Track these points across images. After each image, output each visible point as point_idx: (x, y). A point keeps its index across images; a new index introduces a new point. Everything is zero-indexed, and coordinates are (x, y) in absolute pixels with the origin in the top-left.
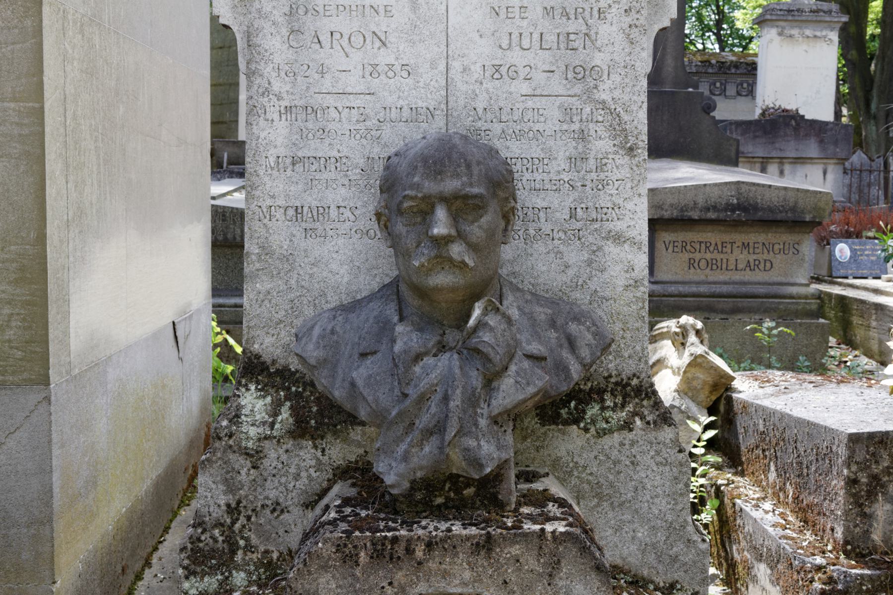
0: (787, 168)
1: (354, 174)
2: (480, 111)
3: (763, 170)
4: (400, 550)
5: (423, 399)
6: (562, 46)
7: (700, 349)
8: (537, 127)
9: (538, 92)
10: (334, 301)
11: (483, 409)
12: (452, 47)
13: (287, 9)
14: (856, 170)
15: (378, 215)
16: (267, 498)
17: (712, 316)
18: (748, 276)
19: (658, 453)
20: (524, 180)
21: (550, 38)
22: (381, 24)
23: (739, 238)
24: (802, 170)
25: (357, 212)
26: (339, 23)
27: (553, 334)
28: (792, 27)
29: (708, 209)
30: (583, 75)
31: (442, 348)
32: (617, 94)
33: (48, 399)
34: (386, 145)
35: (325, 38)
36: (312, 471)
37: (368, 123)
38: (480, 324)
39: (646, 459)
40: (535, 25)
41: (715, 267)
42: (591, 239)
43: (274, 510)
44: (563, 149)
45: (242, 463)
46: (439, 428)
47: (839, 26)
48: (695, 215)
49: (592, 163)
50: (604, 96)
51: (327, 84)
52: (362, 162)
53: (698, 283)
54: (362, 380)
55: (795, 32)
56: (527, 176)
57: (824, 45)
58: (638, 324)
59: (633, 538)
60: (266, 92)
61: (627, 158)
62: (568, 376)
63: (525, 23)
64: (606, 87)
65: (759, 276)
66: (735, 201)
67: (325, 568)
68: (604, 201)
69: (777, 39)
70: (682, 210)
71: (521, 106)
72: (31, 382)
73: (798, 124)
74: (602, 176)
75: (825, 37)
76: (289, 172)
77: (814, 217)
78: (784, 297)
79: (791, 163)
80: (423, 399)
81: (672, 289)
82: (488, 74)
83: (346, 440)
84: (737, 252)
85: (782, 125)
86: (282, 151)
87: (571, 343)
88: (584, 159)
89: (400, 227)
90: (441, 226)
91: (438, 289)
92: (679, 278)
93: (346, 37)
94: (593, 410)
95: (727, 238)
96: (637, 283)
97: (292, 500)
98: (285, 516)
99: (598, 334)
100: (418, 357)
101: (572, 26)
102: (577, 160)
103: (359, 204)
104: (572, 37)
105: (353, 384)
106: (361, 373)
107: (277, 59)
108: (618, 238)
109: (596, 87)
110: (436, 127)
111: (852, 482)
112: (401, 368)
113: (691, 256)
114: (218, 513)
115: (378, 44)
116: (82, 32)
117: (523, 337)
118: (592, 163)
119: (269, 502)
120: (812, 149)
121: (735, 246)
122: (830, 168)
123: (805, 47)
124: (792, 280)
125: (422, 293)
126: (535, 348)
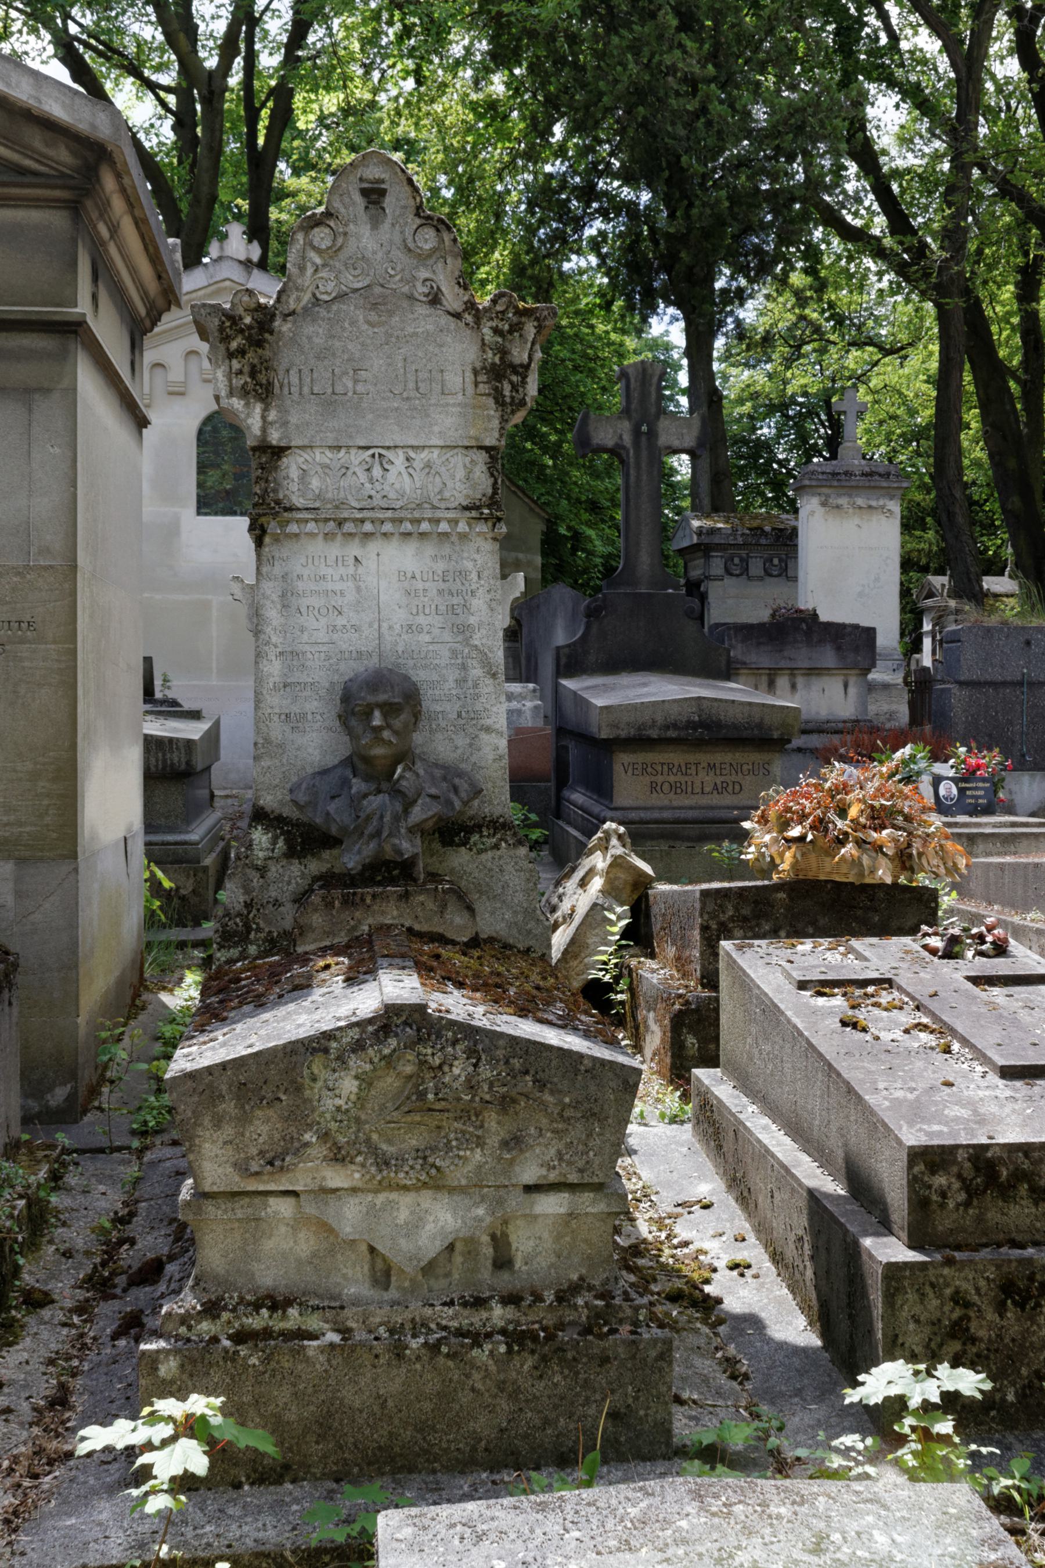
0: (800, 681)
1: (323, 692)
3: (771, 686)
4: (358, 899)
5: (368, 818)
7: (619, 851)
10: (310, 770)
11: (403, 824)
17: (678, 844)
18: (716, 800)
22: (339, 601)
23: (704, 758)
24: (818, 684)
27: (445, 785)
28: (839, 495)
29: (667, 727)
30: (463, 630)
31: (379, 791)
33: (76, 870)
35: (303, 610)
38: (401, 777)
39: (509, 868)
44: (452, 676)
45: (254, 875)
46: (378, 833)
48: (654, 734)
51: (305, 637)
53: (661, 808)
54: (336, 813)
55: (843, 501)
57: (883, 517)
60: (268, 643)
62: (453, 808)
67: (316, 910)
68: (478, 707)
69: (820, 511)
72: (64, 857)
73: (809, 628)
75: (883, 507)
80: (368, 818)
83: (320, 859)
84: (702, 774)
86: (277, 679)
87: (456, 789)
88: (465, 681)
89: (353, 722)
90: (377, 720)
91: (375, 757)
92: (640, 803)
94: (475, 838)
95: (691, 758)
96: (501, 757)
97: (286, 898)
99: (472, 784)
100: (365, 796)
101: (455, 601)
102: (461, 682)
105: (328, 814)
106: (332, 808)
107: (275, 623)
108: (488, 730)
110: (373, 663)
111: (705, 928)
112: (355, 802)
114: (239, 907)
117: (426, 785)
120: (828, 657)
122: (852, 680)
123: (857, 521)
125: (367, 760)
126: (433, 791)
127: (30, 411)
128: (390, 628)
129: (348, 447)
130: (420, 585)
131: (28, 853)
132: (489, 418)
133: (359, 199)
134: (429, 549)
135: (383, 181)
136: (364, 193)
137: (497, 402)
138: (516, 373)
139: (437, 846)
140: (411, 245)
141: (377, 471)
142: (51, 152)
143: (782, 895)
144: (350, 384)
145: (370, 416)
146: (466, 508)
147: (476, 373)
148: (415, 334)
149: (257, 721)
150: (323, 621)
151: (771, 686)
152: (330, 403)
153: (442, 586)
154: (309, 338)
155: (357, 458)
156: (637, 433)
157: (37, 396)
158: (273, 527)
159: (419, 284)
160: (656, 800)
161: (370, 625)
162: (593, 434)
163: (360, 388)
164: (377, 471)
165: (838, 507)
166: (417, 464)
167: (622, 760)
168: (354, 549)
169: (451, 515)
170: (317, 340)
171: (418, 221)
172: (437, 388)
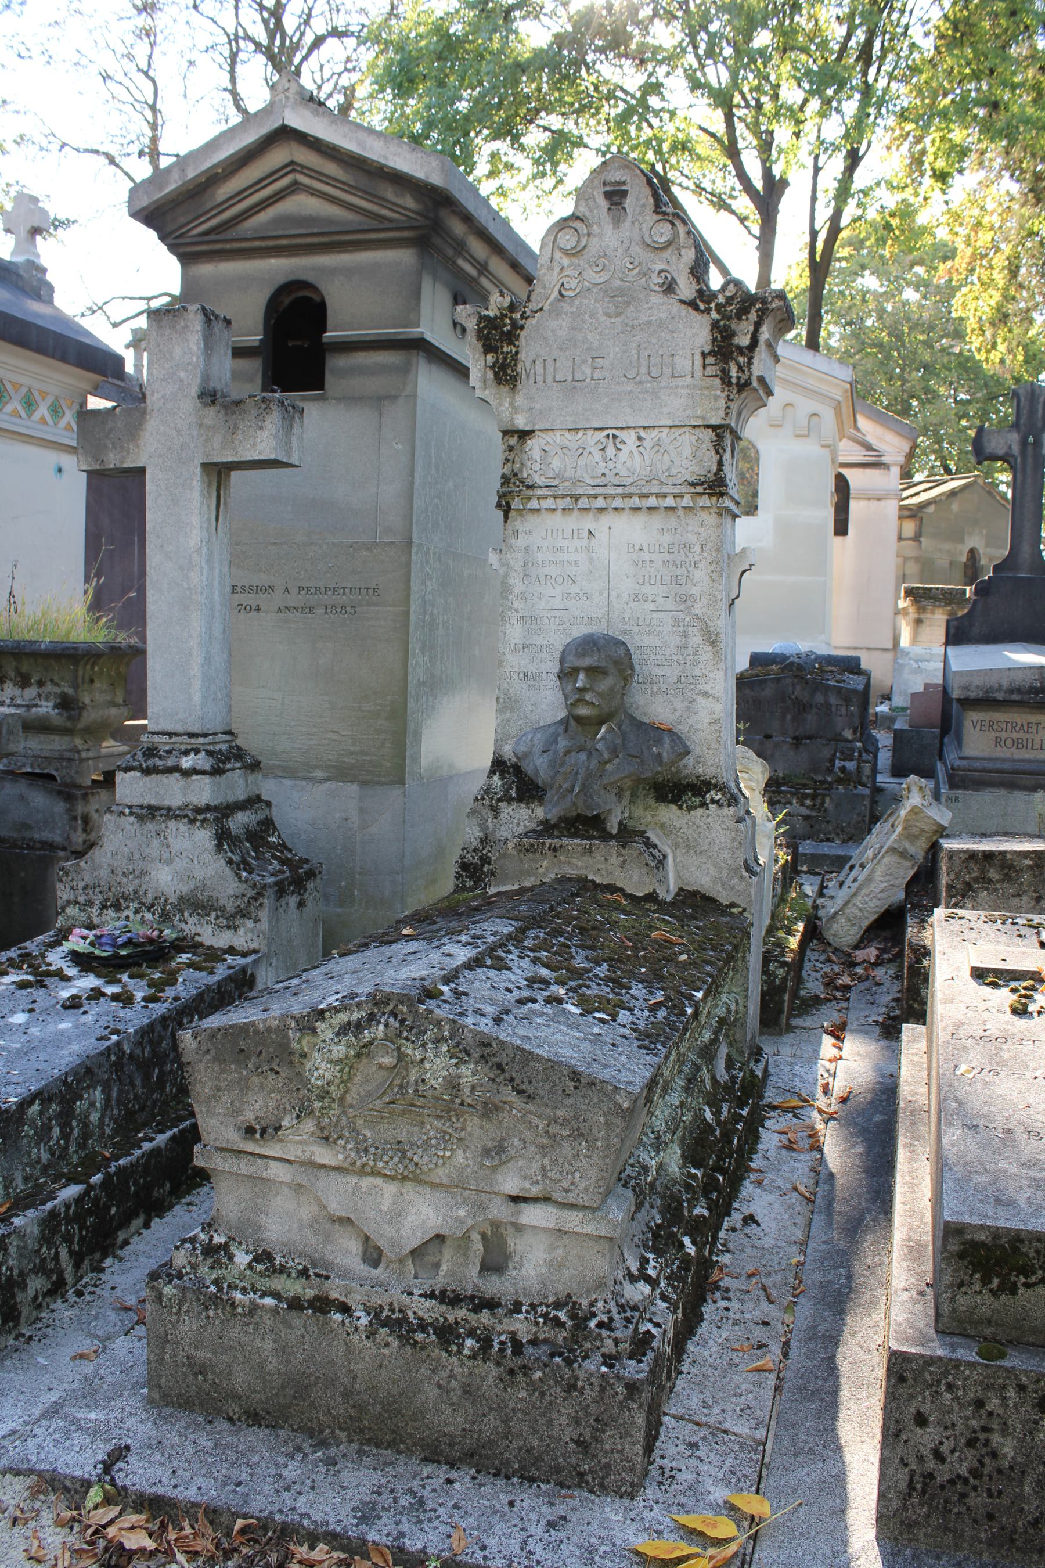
21: (667, 578)
26: (547, 571)
29: (1011, 691)
30: (685, 599)
32: (705, 610)
35: (542, 579)
44: (675, 641)
48: (1000, 696)
50: (698, 612)
51: (542, 604)
54: (539, 766)
56: (653, 657)
60: (510, 608)
68: (697, 673)
70: (987, 692)
81: (978, 765)
86: (518, 641)
99: (685, 746)
108: (706, 694)
116: (440, 560)
127: (381, 415)
128: (619, 596)
130: (647, 557)
131: (369, 778)
133: (604, 203)
134: (657, 521)
135: (624, 183)
136: (608, 195)
137: (723, 382)
138: (742, 353)
139: (651, 802)
140: (648, 241)
141: (610, 451)
142: (400, 201)
144: (588, 372)
145: (605, 400)
146: (693, 485)
147: (704, 355)
152: (572, 387)
154: (553, 331)
156: (1024, 443)
157: (386, 403)
159: (654, 276)
162: (986, 444)
164: (610, 451)
166: (647, 444)
168: (588, 522)
169: (676, 490)
170: (559, 333)
171: (656, 217)
172: (667, 371)
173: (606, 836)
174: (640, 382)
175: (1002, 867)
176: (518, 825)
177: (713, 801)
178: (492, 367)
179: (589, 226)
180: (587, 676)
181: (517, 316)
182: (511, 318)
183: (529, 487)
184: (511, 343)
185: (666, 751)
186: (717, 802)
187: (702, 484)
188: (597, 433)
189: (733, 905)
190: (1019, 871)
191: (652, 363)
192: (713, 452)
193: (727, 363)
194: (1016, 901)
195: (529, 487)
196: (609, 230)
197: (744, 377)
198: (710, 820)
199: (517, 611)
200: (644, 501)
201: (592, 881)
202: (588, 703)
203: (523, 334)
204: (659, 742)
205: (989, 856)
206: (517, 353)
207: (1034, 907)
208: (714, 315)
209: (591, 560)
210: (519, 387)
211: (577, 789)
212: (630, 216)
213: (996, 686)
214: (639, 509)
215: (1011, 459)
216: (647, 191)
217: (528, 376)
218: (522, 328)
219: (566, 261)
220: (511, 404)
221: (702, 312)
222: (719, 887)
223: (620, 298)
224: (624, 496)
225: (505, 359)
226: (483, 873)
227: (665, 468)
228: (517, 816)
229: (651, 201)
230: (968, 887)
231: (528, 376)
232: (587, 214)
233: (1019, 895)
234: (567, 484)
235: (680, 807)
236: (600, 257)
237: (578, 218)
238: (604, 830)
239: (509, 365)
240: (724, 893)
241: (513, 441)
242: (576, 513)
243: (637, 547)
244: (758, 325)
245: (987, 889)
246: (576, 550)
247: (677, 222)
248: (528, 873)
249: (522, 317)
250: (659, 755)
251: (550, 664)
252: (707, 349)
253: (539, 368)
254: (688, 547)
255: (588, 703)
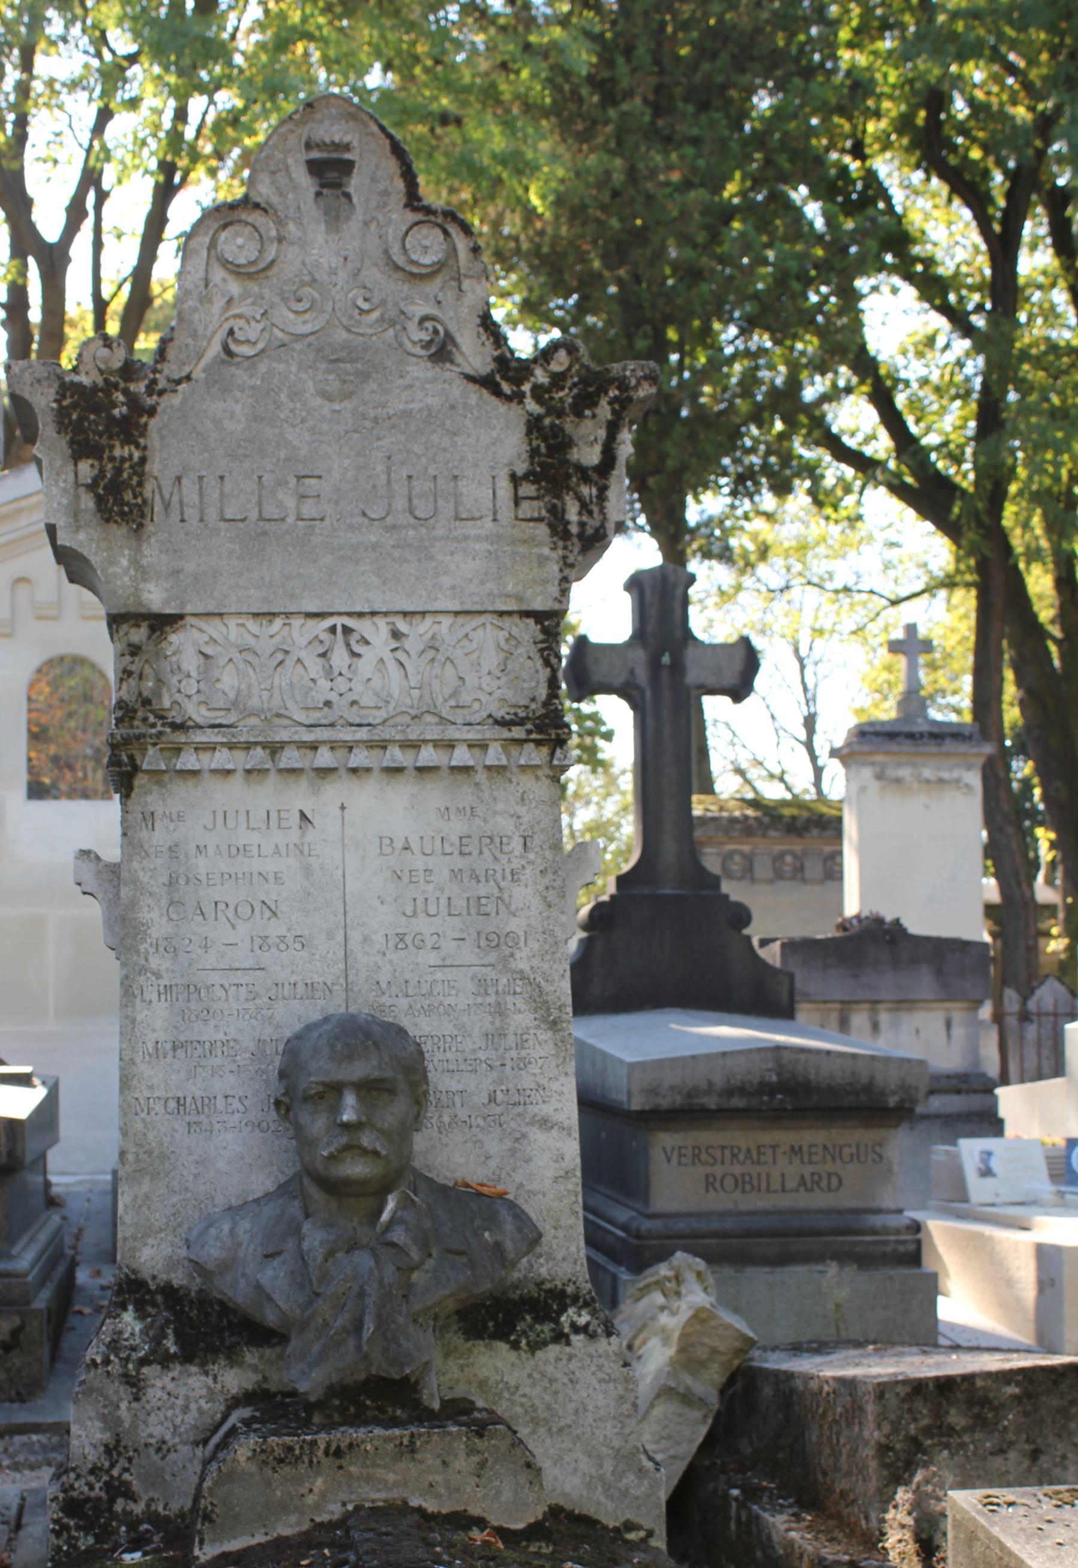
1: (243, 1058)
2: (384, 985)
6: (473, 911)
8: (448, 1001)
9: (448, 962)
12: (350, 915)
13: (165, 879)
14: (1047, 1014)
15: (278, 1103)
16: (151, 1436)
18: (802, 1200)
19: (600, 1368)
20: (435, 1061)
21: (460, 903)
23: (784, 1137)
25: (247, 1102)
26: (218, 893)
28: (899, 765)
30: (497, 943)
32: (535, 962)
34: (278, 1026)
35: (209, 909)
36: (202, 1402)
37: (258, 1002)
40: (442, 890)
41: (748, 1187)
42: (513, 1125)
43: (159, 1449)
44: (480, 1023)
47: (981, 761)
49: (511, 1040)
51: (211, 960)
52: (252, 1046)
54: (266, 1283)
55: (905, 773)
58: (572, 1221)
59: (576, 1470)
60: (143, 970)
61: (550, 1033)
63: (431, 887)
64: (523, 954)
65: (822, 1200)
66: (774, 1078)
68: (527, 1082)
70: (689, 1096)
71: (429, 978)
74: (523, 1053)
75: (958, 781)
76: (169, 1059)
77: (902, 1101)
78: (863, 1232)
79: (890, 1010)
81: (681, 1226)
82: (391, 944)
85: (877, 949)
86: (162, 1036)
88: (503, 1035)
93: (232, 907)
98: (172, 1456)
103: (249, 1093)
104: (483, 901)
108: (545, 1124)
109: (512, 955)
110: (336, 1005)
113: (709, 1170)
115: (268, 913)
118: (511, 1040)
119: (153, 1441)
120: (925, 982)
121: (779, 1151)
124: (874, 1205)
128: (366, 939)
129: (288, 615)
130: (419, 862)
132: (542, 561)
133: (306, 183)
134: (435, 795)
135: (347, 147)
136: (315, 168)
137: (554, 531)
139: (458, 1340)
140: (400, 260)
141: (340, 658)
143: (1012, 1390)
144: (291, 503)
145: (328, 559)
148: (407, 414)
149: (125, 1109)
150: (243, 929)
151: (844, 1025)
153: (459, 862)
154: (217, 422)
155: (303, 634)
156: (655, 665)
158: (151, 759)
160: (717, 1201)
161: (330, 936)
163: (309, 509)
165: (898, 781)
166: (412, 644)
167: (665, 1142)
168: (299, 797)
169: (473, 735)
171: (412, 217)
172: (447, 508)
173: (423, 1416)
174: (394, 527)
175: (970, 1403)
176: (185, 1409)
177: (576, 1329)
178: (92, 487)
179: (280, 223)
180: (360, 1099)
181: (139, 387)
182: (126, 392)
183: (177, 727)
184: (129, 439)
185: (508, 1235)
186: (584, 1329)
187: (521, 722)
188: (311, 623)
189: (629, 1526)
190: (999, 1409)
191: (417, 490)
192: (539, 663)
193: (559, 497)
194: (997, 1462)
195: (177, 727)
196: (318, 233)
197: (592, 523)
198: (574, 1365)
199: (158, 975)
200: (205, 757)
201: (420, 1510)
202: (364, 1152)
203: (154, 423)
204: (492, 1220)
205: (946, 1385)
206: (143, 460)
207: (1029, 1470)
208: (532, 406)
209: (307, 870)
210: (150, 528)
211: (369, 1327)
212: (359, 210)
213: (704, 1085)
214: (399, 770)
215: (635, 693)
216: (392, 166)
217: (167, 506)
218: (152, 412)
219: (234, 288)
220: (135, 562)
221: (509, 399)
222: (599, 1495)
223: (349, 365)
224: (370, 745)
225: (119, 471)
226: (114, 1516)
227: (448, 691)
228: (183, 1391)
229: (400, 185)
230: (915, 1444)
231: (167, 506)
232: (275, 200)
233: (1002, 1451)
234: (254, 721)
235: (515, 1346)
236: (303, 284)
237: (257, 206)
238: (417, 1404)
239: (126, 484)
240: (610, 1506)
241: (139, 635)
242: (273, 778)
243: (399, 844)
244: (613, 428)
245: (947, 1446)
246: (277, 851)
247: (453, 230)
248: (284, 1508)
249: (150, 389)
250: (498, 1246)
251: (231, 1079)
252: (521, 468)
253: (189, 491)
254: (496, 842)
255: (364, 1152)
